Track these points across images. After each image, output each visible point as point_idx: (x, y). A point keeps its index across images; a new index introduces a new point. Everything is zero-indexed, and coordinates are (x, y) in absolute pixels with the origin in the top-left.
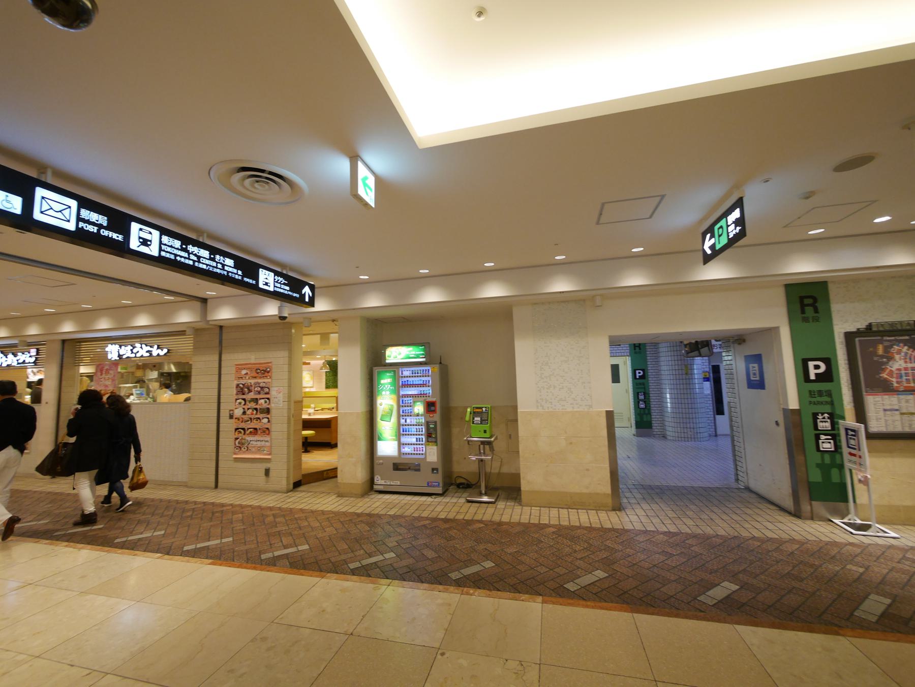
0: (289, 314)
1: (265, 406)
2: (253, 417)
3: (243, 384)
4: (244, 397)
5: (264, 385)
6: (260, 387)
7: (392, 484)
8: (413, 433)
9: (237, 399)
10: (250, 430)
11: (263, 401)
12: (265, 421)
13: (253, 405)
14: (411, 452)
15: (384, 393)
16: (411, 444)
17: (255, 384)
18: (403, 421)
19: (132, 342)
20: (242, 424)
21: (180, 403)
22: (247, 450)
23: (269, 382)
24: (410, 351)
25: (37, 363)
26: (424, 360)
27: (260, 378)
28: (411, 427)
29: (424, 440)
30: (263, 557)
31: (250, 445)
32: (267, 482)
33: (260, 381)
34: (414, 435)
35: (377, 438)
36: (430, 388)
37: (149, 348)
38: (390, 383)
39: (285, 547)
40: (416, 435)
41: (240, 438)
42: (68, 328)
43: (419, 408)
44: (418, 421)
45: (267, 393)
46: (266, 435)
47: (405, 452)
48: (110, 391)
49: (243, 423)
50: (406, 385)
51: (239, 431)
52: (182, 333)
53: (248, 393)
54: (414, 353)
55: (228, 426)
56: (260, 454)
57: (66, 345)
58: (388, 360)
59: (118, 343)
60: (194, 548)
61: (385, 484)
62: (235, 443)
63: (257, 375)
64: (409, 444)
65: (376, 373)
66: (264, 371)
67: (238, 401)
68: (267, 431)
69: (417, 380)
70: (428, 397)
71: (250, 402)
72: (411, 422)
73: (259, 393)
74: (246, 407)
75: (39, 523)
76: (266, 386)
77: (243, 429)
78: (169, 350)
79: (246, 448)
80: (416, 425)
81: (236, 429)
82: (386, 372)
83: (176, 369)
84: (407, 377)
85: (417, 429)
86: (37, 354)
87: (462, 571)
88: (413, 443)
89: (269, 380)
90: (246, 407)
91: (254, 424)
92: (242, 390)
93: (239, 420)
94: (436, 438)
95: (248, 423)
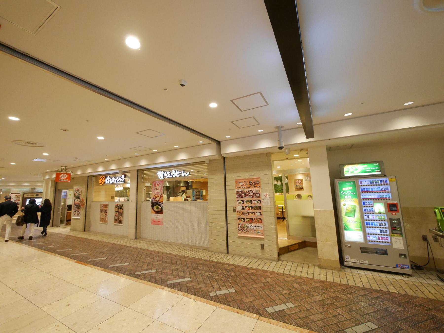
0: (284, 146)
1: (257, 205)
2: (249, 211)
3: (241, 191)
4: (242, 199)
5: (256, 192)
6: (253, 193)
7: (361, 262)
8: (376, 226)
9: (237, 201)
10: (247, 219)
11: (255, 202)
12: (258, 214)
13: (249, 204)
14: (376, 240)
15: (346, 197)
16: (376, 234)
17: (249, 191)
18: (366, 217)
19: (170, 169)
20: (242, 215)
21: (181, 202)
22: (247, 232)
23: (260, 190)
24: (366, 168)
25: (125, 181)
26: (380, 173)
27: (253, 187)
28: (374, 222)
29: (388, 232)
30: (136, 273)
31: (248, 228)
32: (262, 253)
33: (252, 189)
34: (378, 227)
35: (343, 228)
36: (390, 194)
37: (179, 172)
38: (350, 190)
39: (180, 278)
40: (380, 228)
41: (242, 224)
42: (143, 163)
43: (380, 207)
44: (380, 217)
45: (259, 197)
46: (259, 223)
47: (371, 240)
48: (160, 195)
49: (243, 215)
50: (365, 191)
51: (240, 220)
52: (203, 162)
53: (245, 197)
54: (369, 168)
55: (233, 217)
56: (257, 235)
57: (139, 171)
58: (346, 174)
59: (163, 170)
60: (139, 274)
61: (355, 262)
62: (238, 227)
63: (250, 186)
64: (374, 234)
65: (338, 184)
66: (256, 184)
67: (239, 201)
68: (260, 221)
69: (375, 188)
70: (388, 200)
71: (246, 202)
72: (374, 218)
73: (253, 197)
74: (244, 205)
75: (103, 259)
76: (257, 192)
77: (243, 219)
78: (190, 173)
79: (246, 230)
80: (379, 221)
81: (238, 219)
82: (347, 182)
83: (169, 185)
84: (366, 185)
85: (379, 223)
86: (125, 177)
87: (286, 307)
88: (377, 233)
89: (260, 189)
90: (244, 205)
91: (250, 216)
92: (240, 195)
93: (240, 213)
94: (401, 230)
95: (246, 215)
